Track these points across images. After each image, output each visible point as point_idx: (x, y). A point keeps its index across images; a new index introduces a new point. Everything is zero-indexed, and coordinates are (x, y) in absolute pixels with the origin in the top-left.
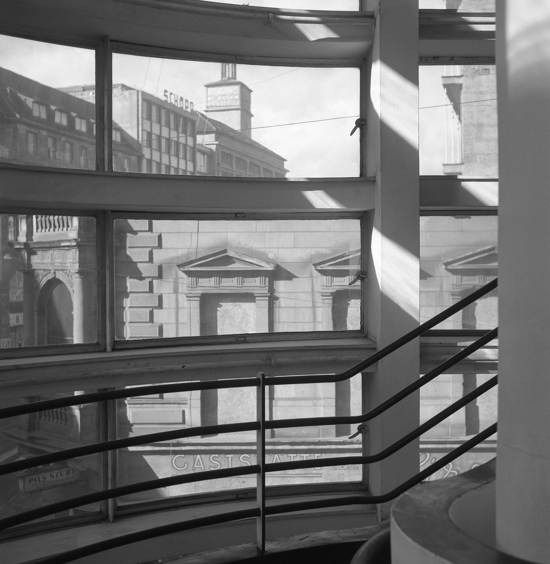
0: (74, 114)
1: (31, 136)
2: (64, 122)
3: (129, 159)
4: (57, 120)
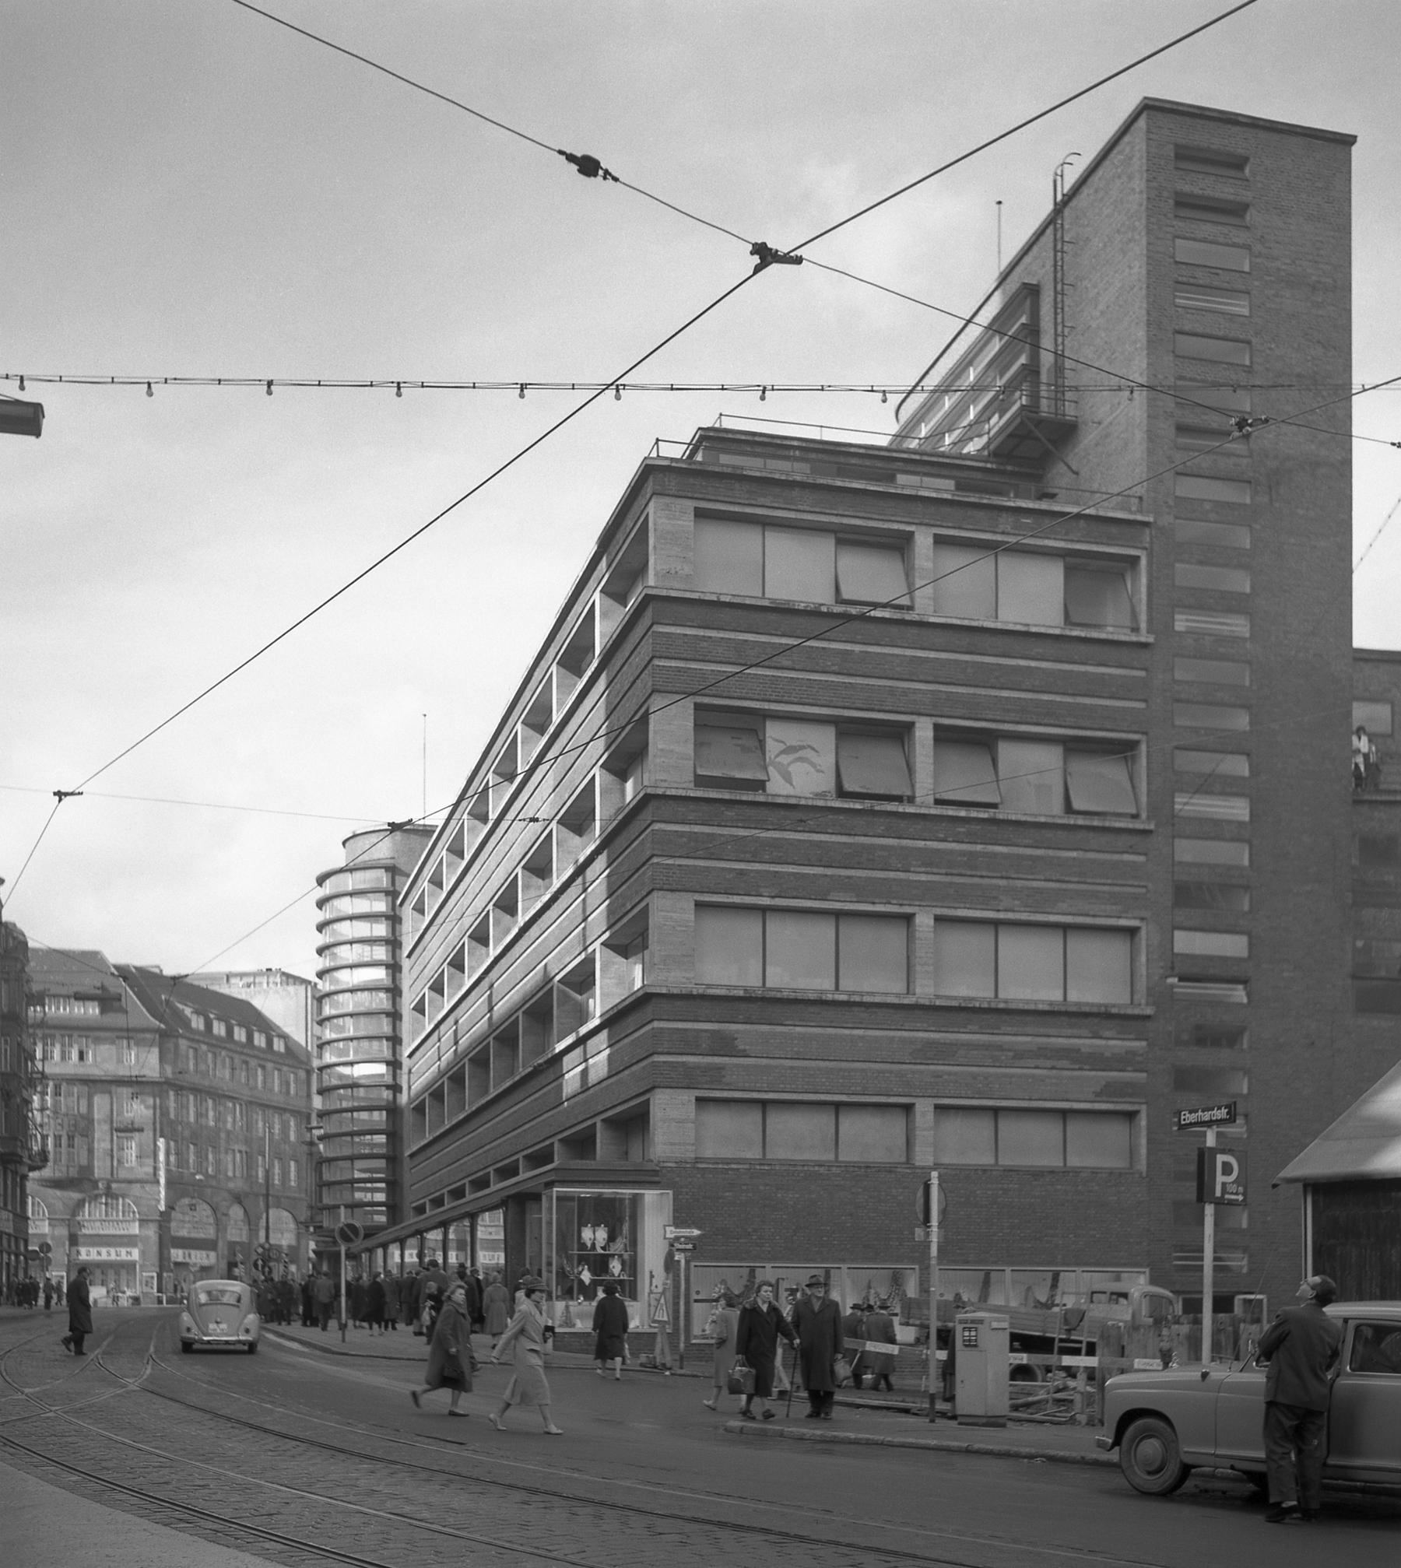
0: (234, 1022)
1: (191, 1052)
2: (223, 1033)
3: (296, 1074)
4: (215, 1031)
